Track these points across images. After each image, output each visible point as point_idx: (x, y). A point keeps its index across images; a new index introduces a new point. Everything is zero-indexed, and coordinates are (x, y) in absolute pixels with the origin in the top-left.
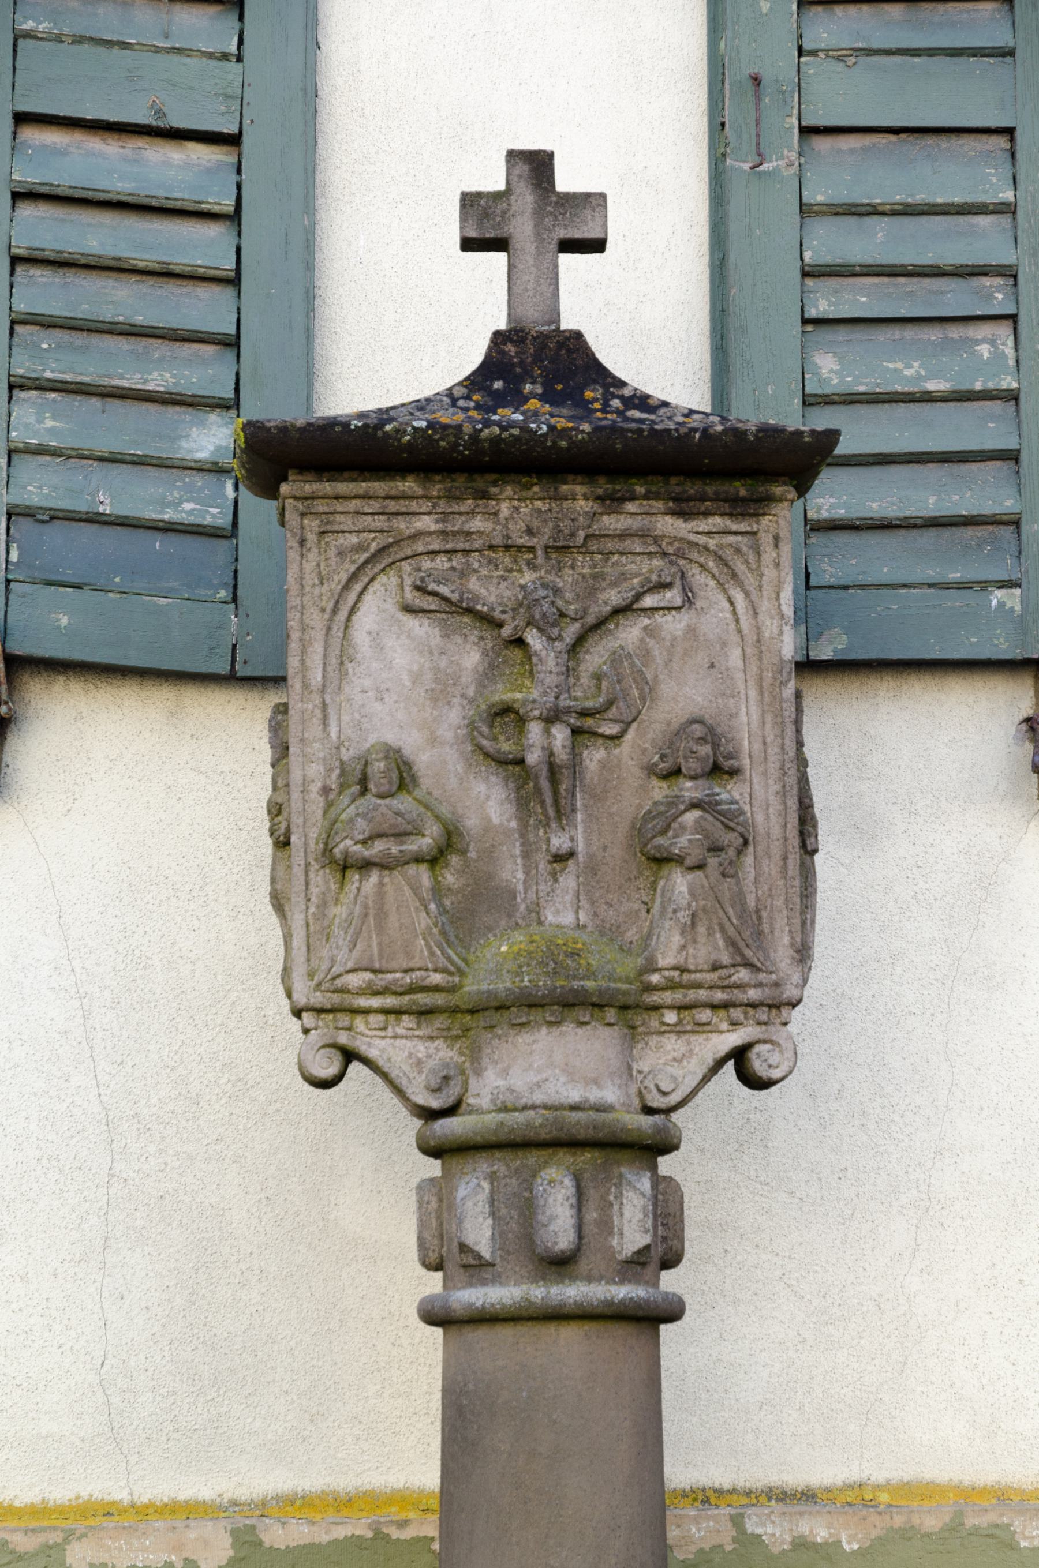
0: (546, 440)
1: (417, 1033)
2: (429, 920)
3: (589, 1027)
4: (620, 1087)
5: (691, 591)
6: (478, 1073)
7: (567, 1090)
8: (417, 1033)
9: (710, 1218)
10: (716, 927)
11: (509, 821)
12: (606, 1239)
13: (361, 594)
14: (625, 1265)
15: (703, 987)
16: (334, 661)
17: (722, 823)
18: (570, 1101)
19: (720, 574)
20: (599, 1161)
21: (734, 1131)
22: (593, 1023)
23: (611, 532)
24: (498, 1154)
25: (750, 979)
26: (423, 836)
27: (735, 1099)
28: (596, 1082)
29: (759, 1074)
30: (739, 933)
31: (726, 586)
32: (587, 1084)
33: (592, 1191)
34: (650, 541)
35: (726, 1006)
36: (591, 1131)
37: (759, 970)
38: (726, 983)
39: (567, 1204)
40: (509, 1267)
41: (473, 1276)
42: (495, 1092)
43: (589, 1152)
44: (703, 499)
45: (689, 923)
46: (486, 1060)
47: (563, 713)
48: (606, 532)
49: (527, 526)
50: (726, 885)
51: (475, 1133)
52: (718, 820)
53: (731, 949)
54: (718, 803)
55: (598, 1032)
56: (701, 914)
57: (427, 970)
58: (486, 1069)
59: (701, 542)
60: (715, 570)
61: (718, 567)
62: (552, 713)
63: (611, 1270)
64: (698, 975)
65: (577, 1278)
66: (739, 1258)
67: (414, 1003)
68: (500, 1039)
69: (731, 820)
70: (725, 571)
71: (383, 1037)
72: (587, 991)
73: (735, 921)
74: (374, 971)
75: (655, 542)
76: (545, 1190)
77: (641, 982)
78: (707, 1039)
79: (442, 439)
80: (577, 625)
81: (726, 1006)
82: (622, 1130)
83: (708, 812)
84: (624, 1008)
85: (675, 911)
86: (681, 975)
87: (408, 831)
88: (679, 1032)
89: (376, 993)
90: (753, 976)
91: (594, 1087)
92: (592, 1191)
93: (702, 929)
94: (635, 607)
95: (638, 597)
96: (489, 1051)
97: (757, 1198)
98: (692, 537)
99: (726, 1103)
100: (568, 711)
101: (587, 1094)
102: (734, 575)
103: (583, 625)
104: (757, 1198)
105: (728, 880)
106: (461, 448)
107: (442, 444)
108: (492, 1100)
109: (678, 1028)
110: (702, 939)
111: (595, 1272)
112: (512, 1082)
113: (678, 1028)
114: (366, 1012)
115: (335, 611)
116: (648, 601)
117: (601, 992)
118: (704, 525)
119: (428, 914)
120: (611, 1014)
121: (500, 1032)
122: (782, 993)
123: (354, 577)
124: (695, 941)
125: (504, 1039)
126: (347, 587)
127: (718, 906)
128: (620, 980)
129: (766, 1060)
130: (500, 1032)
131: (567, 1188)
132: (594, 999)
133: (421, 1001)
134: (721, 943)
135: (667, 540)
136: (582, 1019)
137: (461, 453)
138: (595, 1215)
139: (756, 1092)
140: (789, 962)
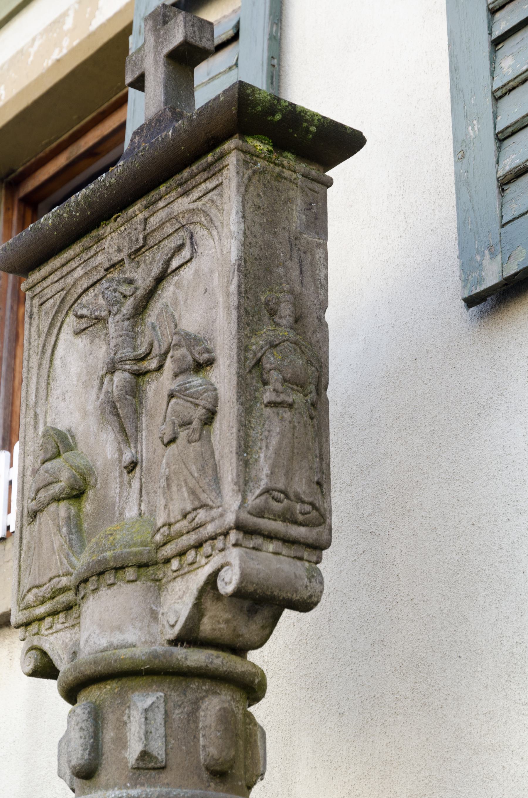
0: (105, 184)
1: (66, 625)
2: (62, 540)
3: (115, 587)
4: (141, 629)
5: (196, 245)
7: (99, 639)
8: (66, 625)
9: (493, 741)
10: (183, 483)
11: (114, 454)
12: (120, 753)
13: (58, 334)
14: (138, 772)
15: (182, 535)
16: (43, 384)
17: (191, 402)
18: (101, 647)
20: (116, 691)
21: (505, 665)
22: (119, 584)
23: (155, 227)
25: (206, 517)
26: (61, 481)
27: (504, 639)
28: (119, 629)
30: (198, 483)
32: (112, 631)
33: (110, 715)
34: (174, 221)
35: (198, 546)
36: (92, 666)
37: (211, 508)
38: (194, 524)
39: (77, 728)
43: (109, 684)
44: (193, 177)
45: (166, 486)
47: (117, 363)
48: (153, 228)
49: (118, 246)
50: (191, 448)
52: (187, 401)
53: (192, 497)
54: (187, 389)
55: (122, 590)
56: (173, 477)
57: (59, 576)
59: (195, 207)
62: (110, 366)
63: (123, 778)
64: (177, 525)
65: (99, 788)
66: (512, 771)
69: (197, 399)
71: (52, 633)
72: (106, 559)
73: (196, 475)
74: (38, 587)
77: (153, 543)
78: (196, 575)
79: (64, 212)
80: (132, 299)
81: (198, 546)
82: (116, 661)
83: (180, 398)
84: (140, 566)
86: (169, 528)
87: (50, 481)
88: (182, 575)
90: (208, 513)
91: (118, 633)
92: (110, 715)
93: (174, 488)
94: (169, 271)
95: (168, 262)
97: (521, 718)
98: (192, 206)
99: (499, 644)
100: (122, 361)
101: (112, 639)
103: (135, 299)
104: (521, 718)
105: (193, 444)
106: (74, 213)
107: (65, 215)
109: (181, 572)
110: (175, 496)
111: (111, 782)
113: (181, 572)
114: (41, 619)
115: (43, 352)
116: (174, 264)
117: (115, 558)
118: (196, 194)
119: (61, 536)
120: (130, 573)
122: (225, 521)
123: (51, 325)
124: (172, 499)
126: (49, 333)
127: (184, 466)
128: (135, 545)
129: (223, 579)
131: (78, 715)
132: (111, 564)
133: (61, 601)
134: (186, 494)
135: (181, 216)
136: (109, 582)
138: (112, 734)
139: (307, 613)
140: (231, 494)
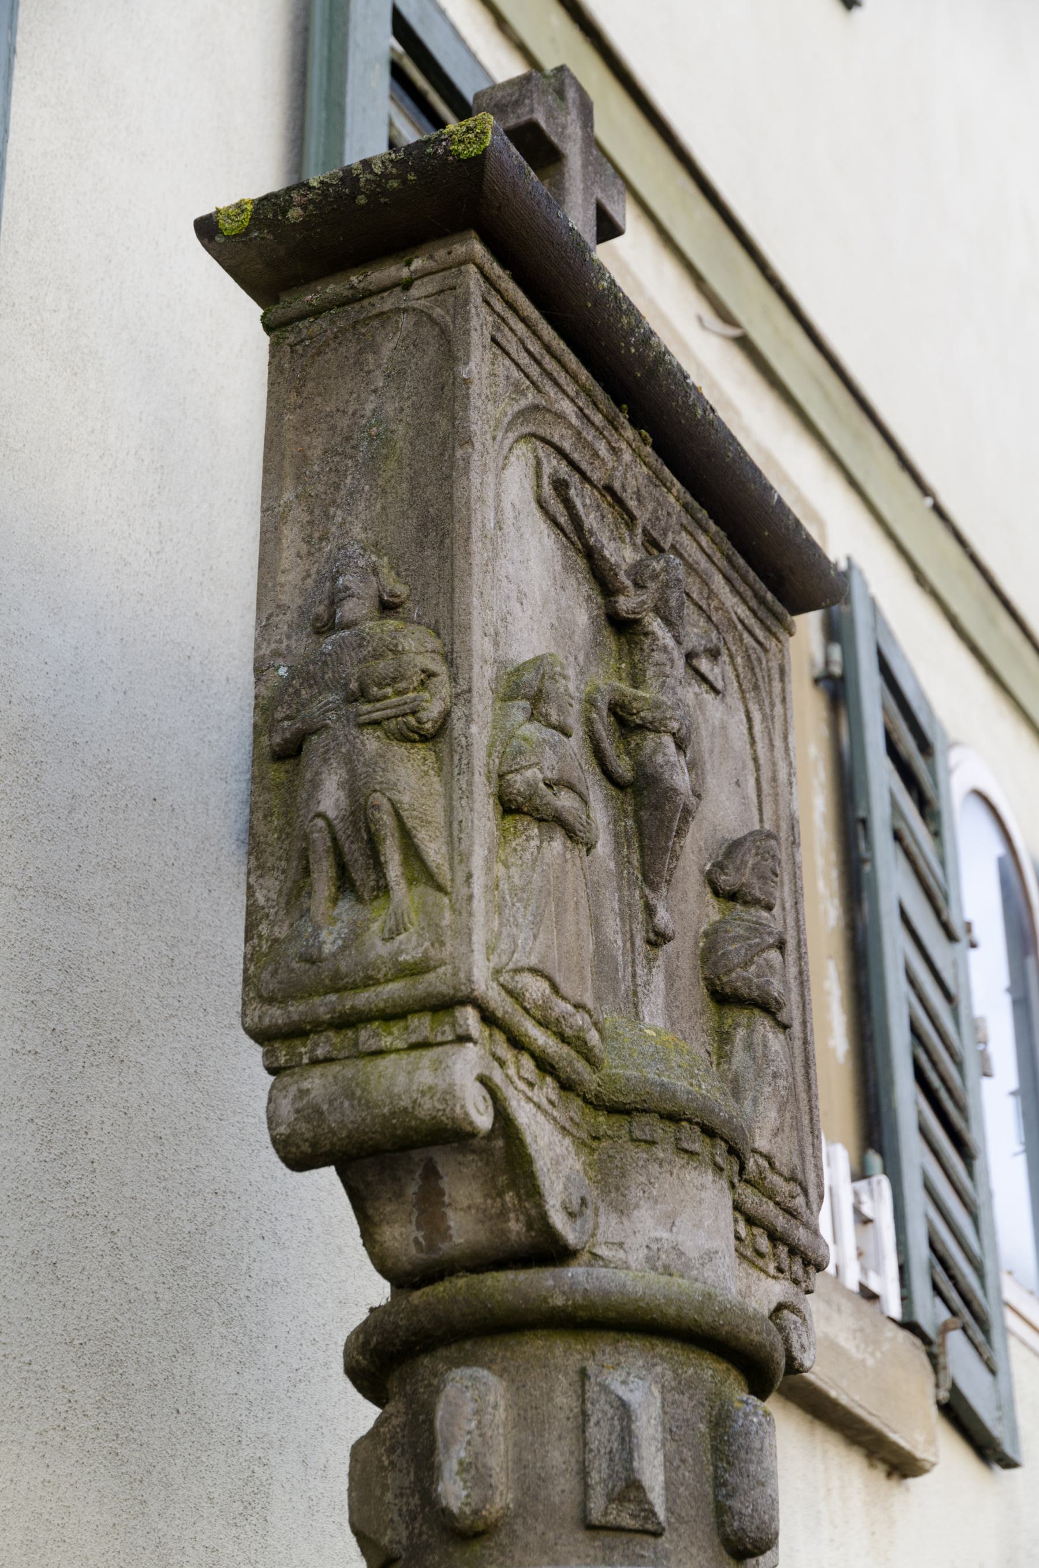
6: (622, 1210)
19: (745, 678)
24: (662, 1348)
29: (462, 1368)
31: (748, 695)
40: (682, 1545)
41: (612, 1549)
42: (654, 1247)
46: (635, 1194)
51: (669, 1301)
58: (637, 1206)
60: (740, 669)
61: (744, 668)
67: (350, 1095)
68: (661, 1166)
70: (749, 677)
75: (708, 598)
76: (760, 1424)
85: (775, 1076)
89: (543, 1023)
96: (643, 1179)
102: (756, 687)
108: (648, 1259)
112: (680, 1238)
121: (661, 1155)
125: (666, 1167)
130: (661, 1155)
137: (628, 344)
